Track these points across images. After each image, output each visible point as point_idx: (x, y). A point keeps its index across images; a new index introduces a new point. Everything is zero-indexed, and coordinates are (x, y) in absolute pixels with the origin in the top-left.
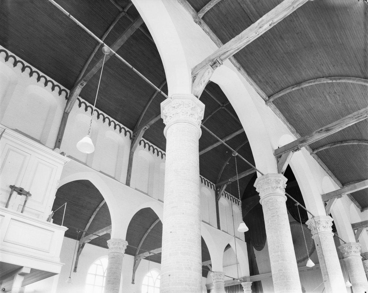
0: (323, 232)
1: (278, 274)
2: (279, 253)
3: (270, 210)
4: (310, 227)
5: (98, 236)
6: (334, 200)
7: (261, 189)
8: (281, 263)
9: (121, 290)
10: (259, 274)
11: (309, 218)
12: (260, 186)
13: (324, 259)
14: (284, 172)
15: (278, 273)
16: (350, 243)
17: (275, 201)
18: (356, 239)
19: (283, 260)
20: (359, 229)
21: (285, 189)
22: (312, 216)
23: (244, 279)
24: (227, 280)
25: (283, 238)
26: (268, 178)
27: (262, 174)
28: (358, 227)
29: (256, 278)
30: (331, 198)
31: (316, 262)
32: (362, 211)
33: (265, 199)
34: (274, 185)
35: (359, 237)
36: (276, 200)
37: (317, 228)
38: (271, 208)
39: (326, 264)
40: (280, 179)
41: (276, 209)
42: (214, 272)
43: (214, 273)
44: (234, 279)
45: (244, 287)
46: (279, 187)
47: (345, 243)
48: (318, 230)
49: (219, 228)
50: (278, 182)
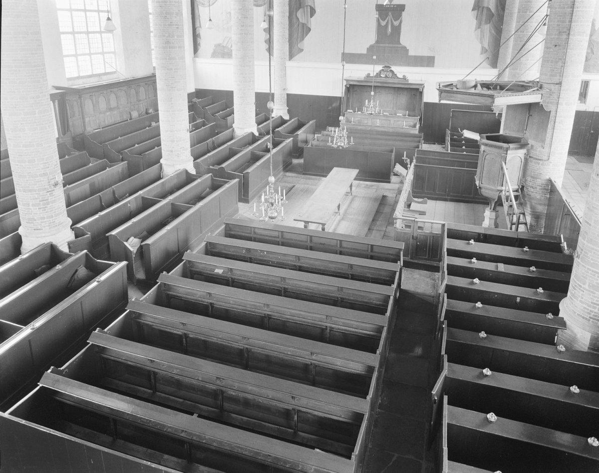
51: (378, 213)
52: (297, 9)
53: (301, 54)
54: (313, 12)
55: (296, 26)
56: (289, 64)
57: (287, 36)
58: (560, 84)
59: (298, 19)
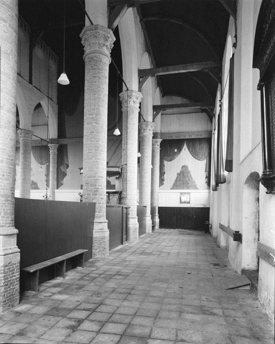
0: (132, 106)
1: (90, 136)
2: (94, 116)
3: (93, 69)
4: (122, 99)
5: (68, 316)
6: (147, 78)
7: (87, 42)
8: (94, 126)
9: (1, 228)
10: (66, 138)
11: (123, 90)
12: (87, 37)
13: (127, 130)
14: (114, 28)
15: (90, 135)
16: (148, 122)
17: (100, 60)
18: (153, 119)
19: (96, 123)
20: (158, 111)
21: (111, 50)
22: (126, 89)
23: (52, 141)
24: (36, 139)
25: (100, 102)
26: (97, 31)
27: (92, 23)
28: (157, 109)
29: (64, 141)
30: (146, 76)
31: (121, 131)
32: (163, 96)
33: (90, 56)
34: (102, 41)
35: (156, 118)
36: (101, 60)
37: (128, 102)
38: (95, 67)
39: (128, 135)
40: (109, 36)
41: (99, 69)
42: (22, 129)
43: (22, 130)
44: (42, 139)
45: (50, 148)
46: (106, 46)
47: (145, 121)
48: (128, 104)
49: (31, 82)
50: (106, 39)
51: (54, 293)
52: (61, 166)
53: (63, 186)
54: (68, 166)
55: (60, 173)
56: (56, 191)
57: (56, 178)
58: (126, 164)
59: (61, 170)
